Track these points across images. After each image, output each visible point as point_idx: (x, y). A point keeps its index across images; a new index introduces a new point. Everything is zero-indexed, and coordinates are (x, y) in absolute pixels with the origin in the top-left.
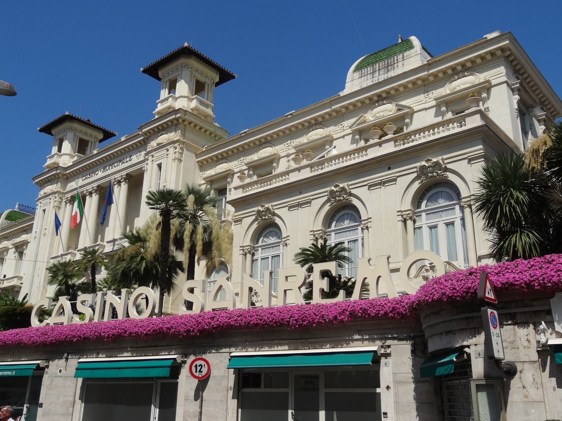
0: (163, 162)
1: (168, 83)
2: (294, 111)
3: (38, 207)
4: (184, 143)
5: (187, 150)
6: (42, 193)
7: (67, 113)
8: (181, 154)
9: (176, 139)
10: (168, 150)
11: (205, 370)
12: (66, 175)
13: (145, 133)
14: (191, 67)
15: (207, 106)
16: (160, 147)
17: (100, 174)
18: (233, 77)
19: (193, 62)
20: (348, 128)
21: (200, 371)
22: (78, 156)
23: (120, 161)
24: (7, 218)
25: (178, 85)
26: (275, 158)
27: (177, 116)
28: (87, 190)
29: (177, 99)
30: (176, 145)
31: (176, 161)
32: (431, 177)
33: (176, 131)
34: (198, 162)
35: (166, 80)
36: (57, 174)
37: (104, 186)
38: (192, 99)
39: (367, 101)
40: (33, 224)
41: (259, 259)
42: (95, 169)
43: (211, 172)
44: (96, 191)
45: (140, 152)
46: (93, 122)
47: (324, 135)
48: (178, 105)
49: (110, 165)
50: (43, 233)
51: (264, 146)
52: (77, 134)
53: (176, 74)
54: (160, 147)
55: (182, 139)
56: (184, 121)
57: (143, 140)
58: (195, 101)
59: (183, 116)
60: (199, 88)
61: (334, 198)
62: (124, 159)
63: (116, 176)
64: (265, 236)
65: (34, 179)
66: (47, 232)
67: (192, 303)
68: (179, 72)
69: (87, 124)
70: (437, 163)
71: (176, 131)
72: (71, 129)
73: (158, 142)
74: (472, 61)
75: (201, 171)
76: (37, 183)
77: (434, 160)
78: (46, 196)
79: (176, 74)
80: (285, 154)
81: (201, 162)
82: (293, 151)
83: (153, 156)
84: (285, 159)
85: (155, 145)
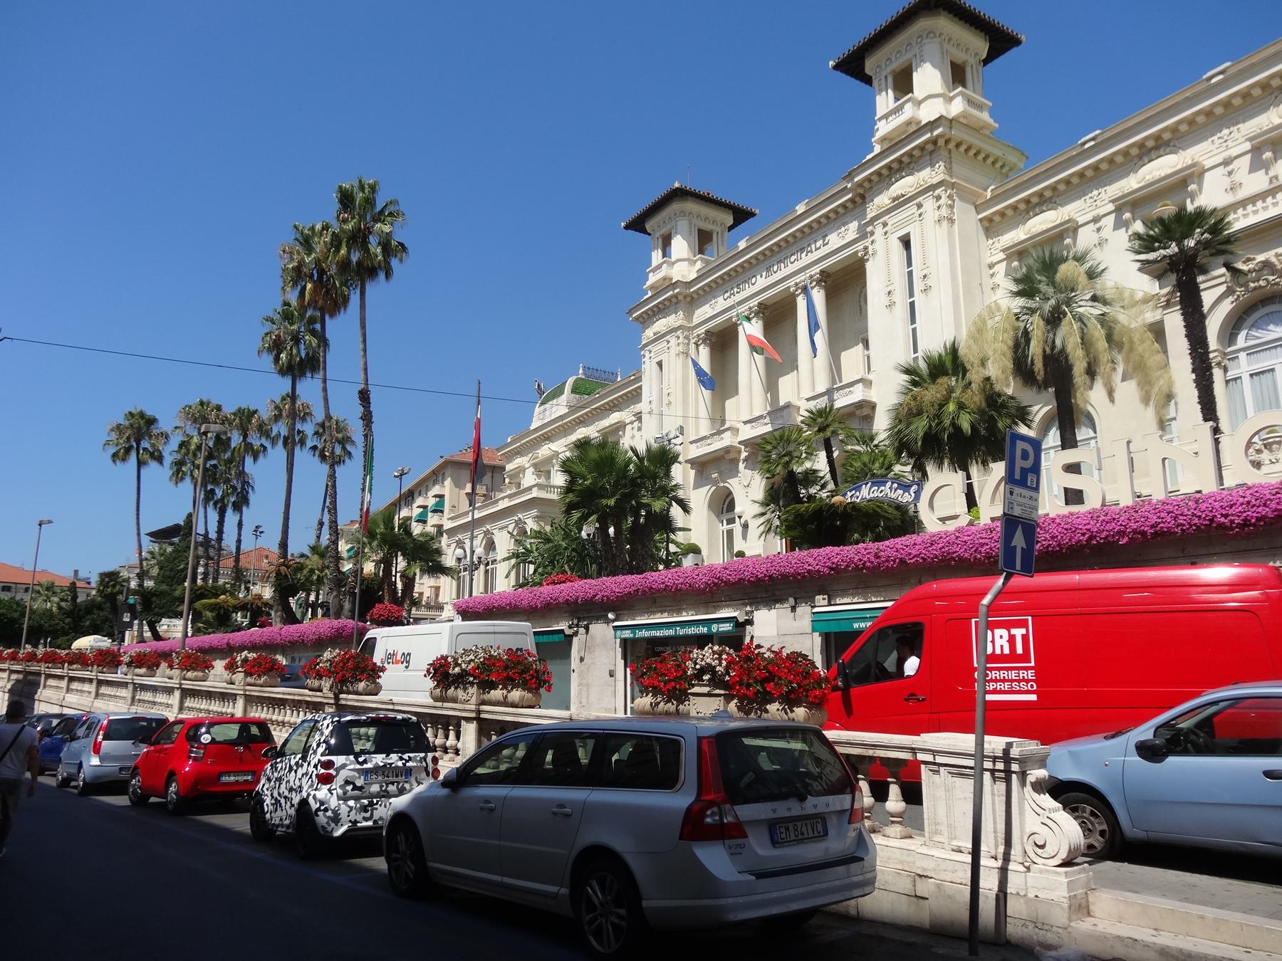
0: (664, 357)
1: (890, 80)
2: (1228, 64)
3: (646, 359)
4: (953, 186)
5: (962, 199)
6: (649, 333)
7: (677, 185)
8: (951, 207)
10: (919, 206)
12: (691, 295)
13: (860, 185)
14: (940, 34)
15: (980, 107)
17: (761, 281)
18: (752, 215)
22: (702, 260)
23: (802, 250)
24: (574, 391)
25: (917, 77)
26: (1192, 174)
27: (935, 133)
28: (796, 284)
29: (919, 103)
30: (937, 192)
31: (945, 223)
32: (1255, 288)
33: (932, 165)
34: (981, 220)
35: (884, 74)
36: (676, 296)
37: (830, 271)
38: (952, 99)
39: (1022, 206)
40: (640, 387)
41: (1246, 378)
42: (749, 274)
43: (1018, 235)
44: (757, 314)
45: (845, 224)
47: (1179, 167)
48: (927, 113)
49: (780, 262)
50: (665, 401)
51: (1153, 154)
52: (694, 221)
53: (909, 55)
55: (948, 178)
56: (947, 142)
57: (852, 200)
58: (959, 99)
59: (947, 131)
60: (957, 75)
61: (1241, 286)
62: (809, 245)
63: (800, 278)
64: (1253, 326)
65: (630, 312)
66: (672, 398)
67: (1081, 492)
68: (916, 50)
70: (1266, 265)
71: (932, 165)
72: (683, 213)
74: (1053, 188)
75: (988, 236)
76: (637, 319)
77: (1261, 258)
78: (659, 337)
79: (909, 55)
80: (1089, 217)
81: (990, 219)
82: (1002, 256)
83: (885, 225)
84: (1092, 226)
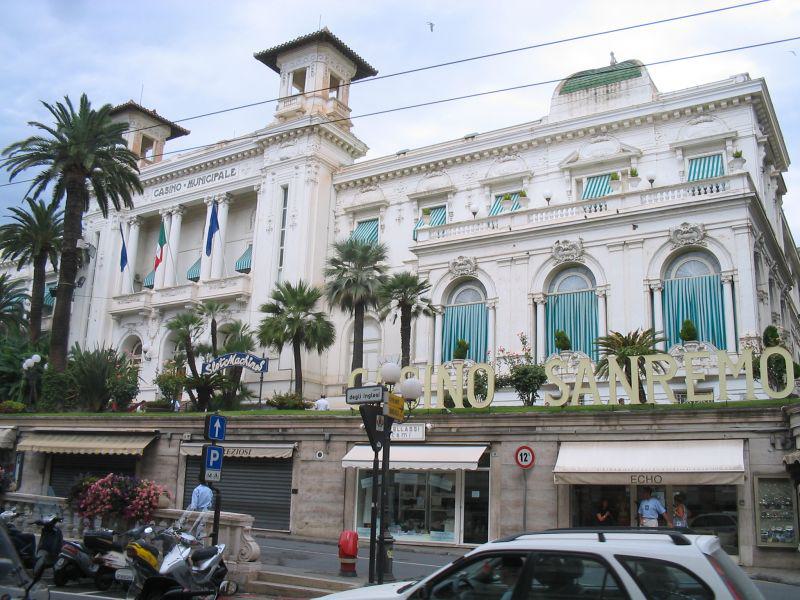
1: (291, 76)
9: (309, 154)
11: (529, 458)
16: (285, 161)
19: (329, 53)
20: (478, 185)
21: (526, 460)
46: (160, 113)
54: (285, 161)
69: (152, 116)
73: (282, 156)
85: (278, 159)
